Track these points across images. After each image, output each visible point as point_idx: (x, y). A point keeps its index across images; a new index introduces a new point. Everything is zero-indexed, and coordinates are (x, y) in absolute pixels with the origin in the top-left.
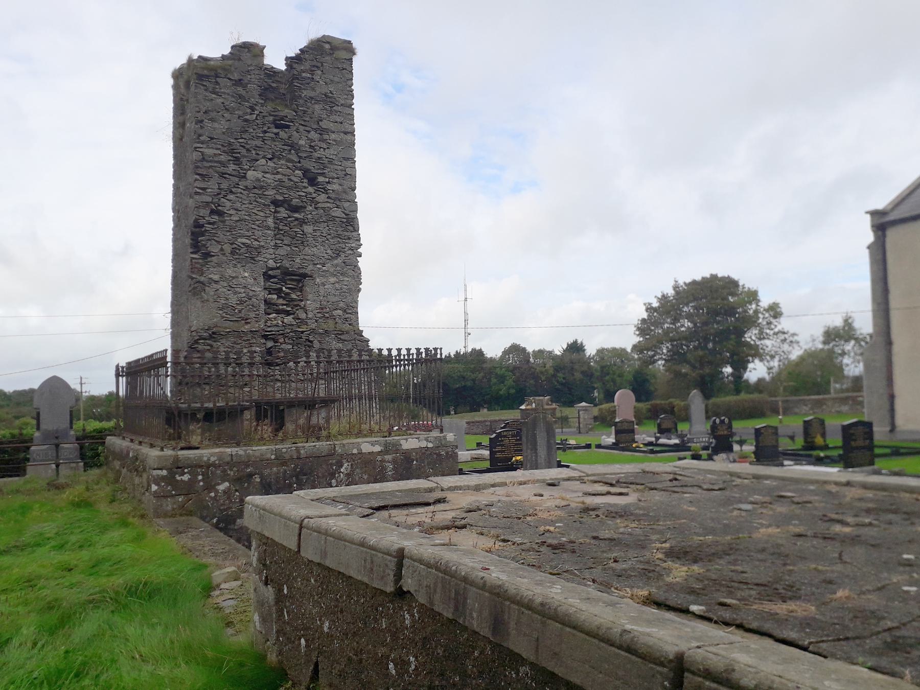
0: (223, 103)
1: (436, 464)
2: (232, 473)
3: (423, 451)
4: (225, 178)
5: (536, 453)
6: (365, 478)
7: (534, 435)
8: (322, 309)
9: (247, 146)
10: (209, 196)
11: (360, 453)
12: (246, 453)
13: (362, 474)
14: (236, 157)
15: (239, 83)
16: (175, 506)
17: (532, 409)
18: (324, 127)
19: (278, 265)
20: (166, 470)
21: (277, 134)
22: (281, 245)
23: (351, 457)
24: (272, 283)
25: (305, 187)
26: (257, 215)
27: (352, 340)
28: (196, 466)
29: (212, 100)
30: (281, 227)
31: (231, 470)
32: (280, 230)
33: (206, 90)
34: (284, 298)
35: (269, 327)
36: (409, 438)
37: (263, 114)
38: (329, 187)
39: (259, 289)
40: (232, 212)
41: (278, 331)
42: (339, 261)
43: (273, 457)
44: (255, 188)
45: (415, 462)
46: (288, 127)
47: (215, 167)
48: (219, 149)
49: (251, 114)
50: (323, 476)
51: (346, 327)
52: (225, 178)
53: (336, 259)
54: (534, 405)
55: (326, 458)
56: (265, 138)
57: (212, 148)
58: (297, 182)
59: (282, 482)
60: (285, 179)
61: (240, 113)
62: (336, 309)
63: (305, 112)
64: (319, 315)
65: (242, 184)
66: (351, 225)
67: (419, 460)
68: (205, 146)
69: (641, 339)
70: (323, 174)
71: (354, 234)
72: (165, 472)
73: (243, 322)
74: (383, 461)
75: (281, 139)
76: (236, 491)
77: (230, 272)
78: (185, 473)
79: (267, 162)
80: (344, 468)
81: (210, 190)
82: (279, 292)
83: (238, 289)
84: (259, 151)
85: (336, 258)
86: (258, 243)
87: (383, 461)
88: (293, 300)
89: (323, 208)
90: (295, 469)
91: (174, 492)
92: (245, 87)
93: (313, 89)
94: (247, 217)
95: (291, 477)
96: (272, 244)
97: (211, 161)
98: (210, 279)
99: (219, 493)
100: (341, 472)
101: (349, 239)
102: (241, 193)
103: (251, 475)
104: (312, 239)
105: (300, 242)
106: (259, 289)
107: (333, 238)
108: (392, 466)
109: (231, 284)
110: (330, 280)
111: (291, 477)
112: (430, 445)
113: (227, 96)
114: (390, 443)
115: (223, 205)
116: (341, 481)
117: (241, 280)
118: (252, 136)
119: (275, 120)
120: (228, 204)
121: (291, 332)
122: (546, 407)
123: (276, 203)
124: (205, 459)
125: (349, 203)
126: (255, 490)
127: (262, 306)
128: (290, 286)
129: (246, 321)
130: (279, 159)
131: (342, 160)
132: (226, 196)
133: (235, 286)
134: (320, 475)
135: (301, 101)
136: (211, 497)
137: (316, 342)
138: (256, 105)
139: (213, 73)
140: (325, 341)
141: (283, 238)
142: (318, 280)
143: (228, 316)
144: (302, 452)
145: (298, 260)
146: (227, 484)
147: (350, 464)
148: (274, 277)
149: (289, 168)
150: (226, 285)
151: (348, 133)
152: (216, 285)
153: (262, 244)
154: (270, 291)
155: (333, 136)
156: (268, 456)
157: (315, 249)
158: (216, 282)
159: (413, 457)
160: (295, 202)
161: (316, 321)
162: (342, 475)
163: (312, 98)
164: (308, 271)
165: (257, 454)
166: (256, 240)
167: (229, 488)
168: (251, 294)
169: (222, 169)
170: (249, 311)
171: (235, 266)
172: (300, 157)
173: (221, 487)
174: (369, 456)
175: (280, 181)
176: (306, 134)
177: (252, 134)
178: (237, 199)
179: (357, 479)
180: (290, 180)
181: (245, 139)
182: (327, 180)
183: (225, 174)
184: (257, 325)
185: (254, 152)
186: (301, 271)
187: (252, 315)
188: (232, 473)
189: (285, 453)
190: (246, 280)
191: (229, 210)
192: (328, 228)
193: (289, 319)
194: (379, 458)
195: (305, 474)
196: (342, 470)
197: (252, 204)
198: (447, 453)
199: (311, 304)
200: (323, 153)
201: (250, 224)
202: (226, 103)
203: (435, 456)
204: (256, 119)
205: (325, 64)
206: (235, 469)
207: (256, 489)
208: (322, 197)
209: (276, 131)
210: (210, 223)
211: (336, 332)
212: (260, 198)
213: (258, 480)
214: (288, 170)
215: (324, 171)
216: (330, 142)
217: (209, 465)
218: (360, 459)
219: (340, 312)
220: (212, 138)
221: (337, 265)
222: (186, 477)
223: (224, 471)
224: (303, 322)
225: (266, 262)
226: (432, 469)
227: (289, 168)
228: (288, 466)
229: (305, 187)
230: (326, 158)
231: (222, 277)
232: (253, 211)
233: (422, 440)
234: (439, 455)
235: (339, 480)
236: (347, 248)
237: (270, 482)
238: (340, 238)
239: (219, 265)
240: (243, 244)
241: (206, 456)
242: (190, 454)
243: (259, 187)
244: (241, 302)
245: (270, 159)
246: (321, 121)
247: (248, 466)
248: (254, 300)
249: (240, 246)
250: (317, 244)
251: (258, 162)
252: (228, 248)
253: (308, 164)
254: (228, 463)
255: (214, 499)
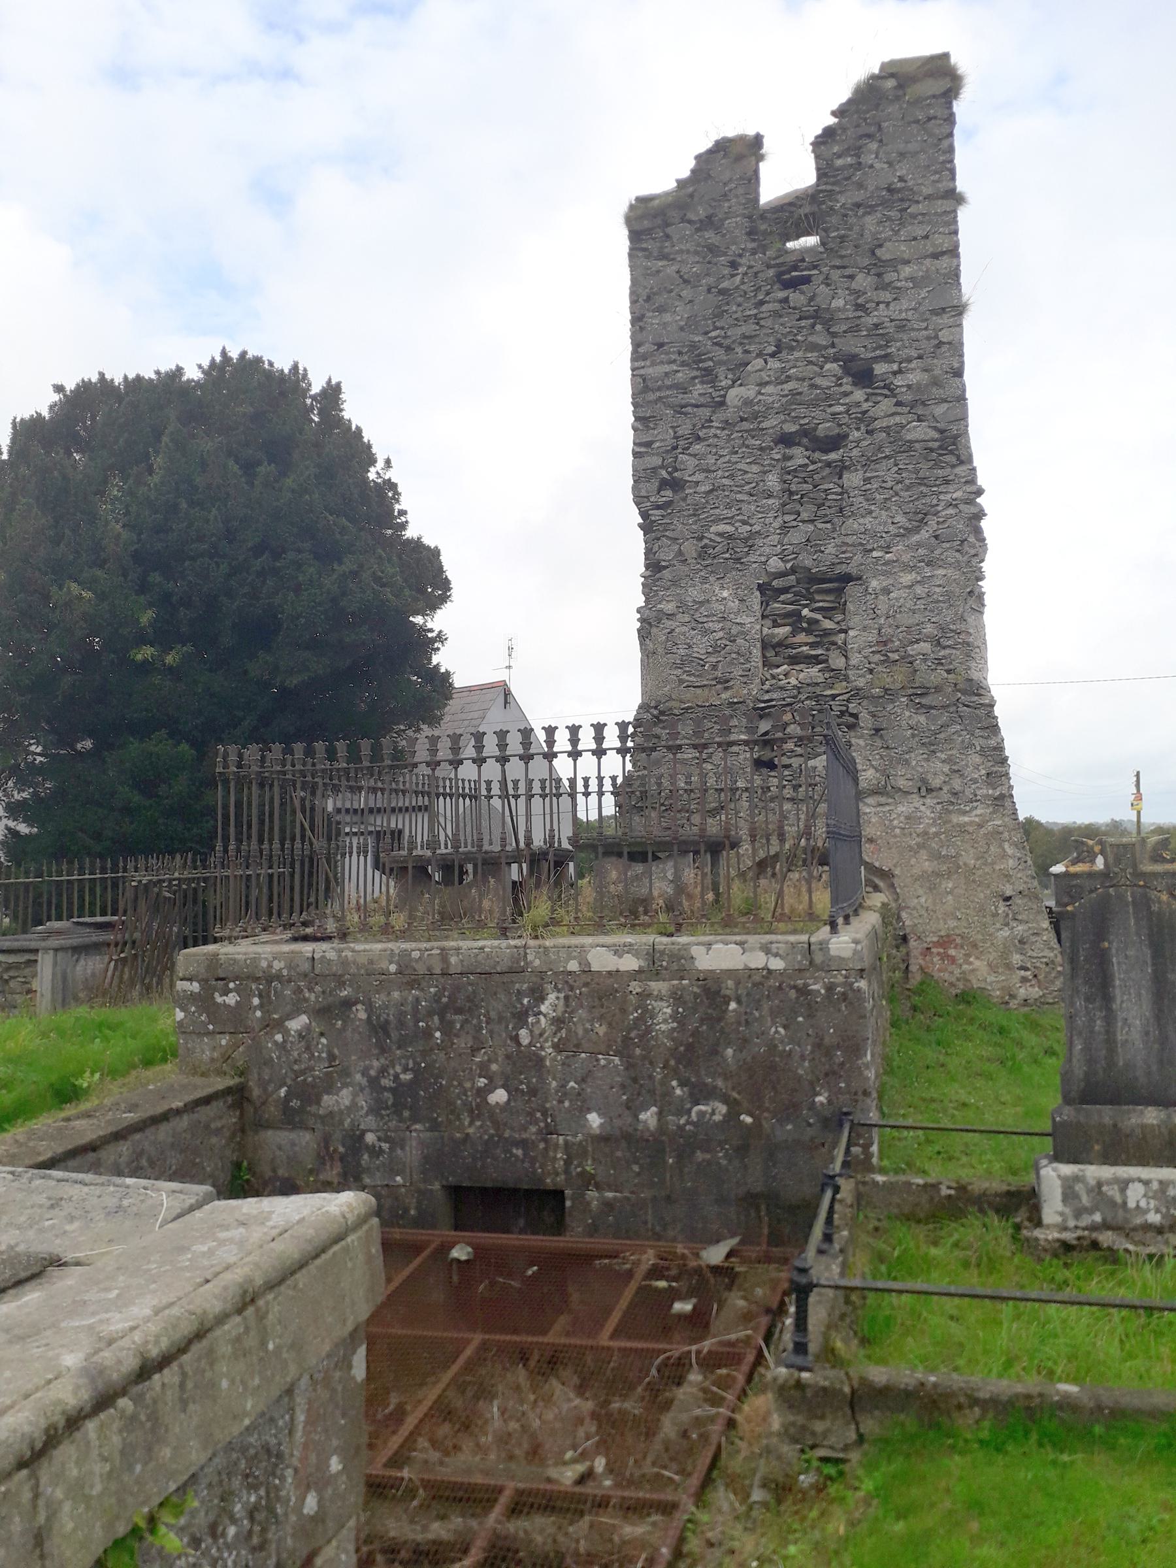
0: (678, 272)
1: (797, 1014)
2: (313, 997)
3: (757, 978)
4: (685, 414)
5: (1109, 1010)
6: (601, 1034)
7: (1102, 960)
8: (885, 643)
9: (727, 342)
10: (658, 454)
11: (586, 970)
12: (340, 956)
13: (592, 1021)
14: (705, 369)
15: (709, 222)
16: (216, 1055)
17: (1091, 875)
18: (887, 257)
19: (789, 565)
20: (199, 982)
21: (786, 300)
22: (795, 523)
23: (566, 981)
24: (783, 603)
25: (846, 394)
26: (746, 472)
27: (948, 706)
28: (248, 977)
29: (658, 272)
30: (794, 488)
31: (311, 990)
32: (791, 493)
33: (647, 257)
34: (809, 632)
35: (768, 692)
36: (717, 942)
37: (755, 269)
38: (899, 381)
39: (749, 620)
40: (699, 477)
41: (784, 699)
42: (924, 534)
43: (393, 968)
44: (742, 419)
45: (733, 1005)
46: (807, 280)
47: (667, 397)
48: (674, 361)
49: (733, 276)
50: (501, 1019)
51: (937, 677)
52: (685, 414)
53: (918, 533)
54: (1100, 863)
55: (505, 978)
56: (762, 315)
57: (662, 362)
58: (829, 388)
59: (411, 1024)
60: (804, 387)
61: (711, 280)
62: (917, 641)
63: (843, 239)
64: (878, 657)
65: (719, 416)
66: (951, 452)
67: (744, 999)
68: (648, 363)
69: (418, 620)
70: (887, 358)
71: (960, 470)
72: (195, 987)
73: (719, 686)
74: (644, 995)
75: (794, 308)
76: (322, 1034)
77: (694, 593)
78: (230, 991)
79: (766, 362)
80: (547, 1003)
81: (657, 444)
82: (794, 618)
83: (711, 624)
84: (750, 344)
85: (917, 530)
86: (749, 528)
87: (644, 995)
88: (827, 633)
89: (886, 430)
90: (437, 998)
91: (211, 1027)
92: (718, 229)
93: (861, 186)
94: (726, 481)
95: (430, 1014)
96: (776, 524)
97: (659, 389)
98: (661, 611)
99: (290, 1035)
100: (540, 1013)
101: (947, 482)
102: (715, 436)
103: (348, 1004)
104: (861, 499)
105: (833, 510)
106: (749, 620)
107: (908, 489)
108: (669, 1011)
109: (697, 616)
110: (901, 580)
111: (430, 1014)
112: (777, 964)
113: (684, 257)
114: (662, 953)
115: (682, 467)
116: (541, 1035)
117: (715, 606)
118: (736, 319)
119: (779, 275)
120: (691, 463)
121: (807, 698)
122: (1149, 868)
123: (786, 440)
124: (264, 964)
125: (946, 405)
126: (357, 1037)
127: (757, 652)
128: (821, 604)
129: (725, 683)
130: (792, 349)
131: (928, 314)
132: (688, 448)
133: (705, 619)
134: (493, 1014)
135: (834, 220)
136: (276, 1043)
137: (864, 715)
138: (740, 256)
139: (659, 221)
140: (884, 713)
141: (798, 507)
142: (874, 583)
143: (692, 679)
144: (453, 960)
145: (830, 549)
146: (304, 1019)
147: (562, 995)
148: (785, 590)
149: (811, 363)
150: (687, 620)
151: (943, 253)
152: (671, 622)
153: (757, 528)
154: (774, 621)
155: (907, 271)
156: (384, 965)
157: (869, 519)
158: (670, 616)
159: (728, 992)
160: (825, 428)
161: (871, 671)
162: (541, 1017)
163: (858, 205)
164: (852, 569)
165: (362, 960)
166: (744, 523)
167: (308, 1028)
168: (735, 630)
169: (681, 398)
170: (731, 663)
171: (705, 580)
172: (834, 335)
173: (296, 1024)
174: (609, 981)
175: (795, 393)
176: (845, 283)
177: (735, 316)
178: (709, 449)
179: (580, 1032)
180: (813, 386)
181: (722, 328)
182: (895, 367)
183: (685, 406)
184: (745, 692)
185: (739, 350)
186: (838, 570)
187: (737, 672)
188: (313, 997)
189: (417, 961)
190: (725, 606)
191: (693, 474)
192: (896, 469)
193: (813, 673)
194: (635, 987)
195: (459, 1011)
196: (543, 1008)
197: (736, 452)
198: (830, 988)
199: (859, 638)
200: (885, 313)
201: (733, 495)
202: (684, 270)
203: (793, 994)
204: (743, 283)
205: (884, 125)
206: (318, 988)
207: (360, 1033)
208: (886, 405)
209: (781, 295)
210: (658, 507)
211: (910, 691)
212: (753, 437)
213: (363, 1015)
214: (809, 367)
215: (889, 351)
216: (899, 284)
217: (270, 978)
218: (586, 985)
219: (925, 647)
220: (660, 345)
221: (919, 545)
222: (232, 999)
223: (299, 990)
224: (837, 675)
225: (765, 563)
226: (785, 1027)
227: (811, 363)
228: (422, 990)
229: (846, 394)
230: (892, 321)
231: (682, 606)
232: (739, 466)
233: (752, 949)
234: (803, 991)
235: (537, 1032)
236: (943, 504)
237: (387, 1022)
238: (925, 485)
239: (675, 583)
240: (720, 535)
241: (266, 959)
242: (239, 954)
243: (752, 414)
244: (716, 649)
245: (773, 355)
246: (880, 246)
247: (342, 984)
248: (740, 641)
249: (714, 541)
250: (873, 508)
251: (749, 367)
252: (690, 548)
253: (855, 345)
254: (306, 976)
255: (282, 1046)
